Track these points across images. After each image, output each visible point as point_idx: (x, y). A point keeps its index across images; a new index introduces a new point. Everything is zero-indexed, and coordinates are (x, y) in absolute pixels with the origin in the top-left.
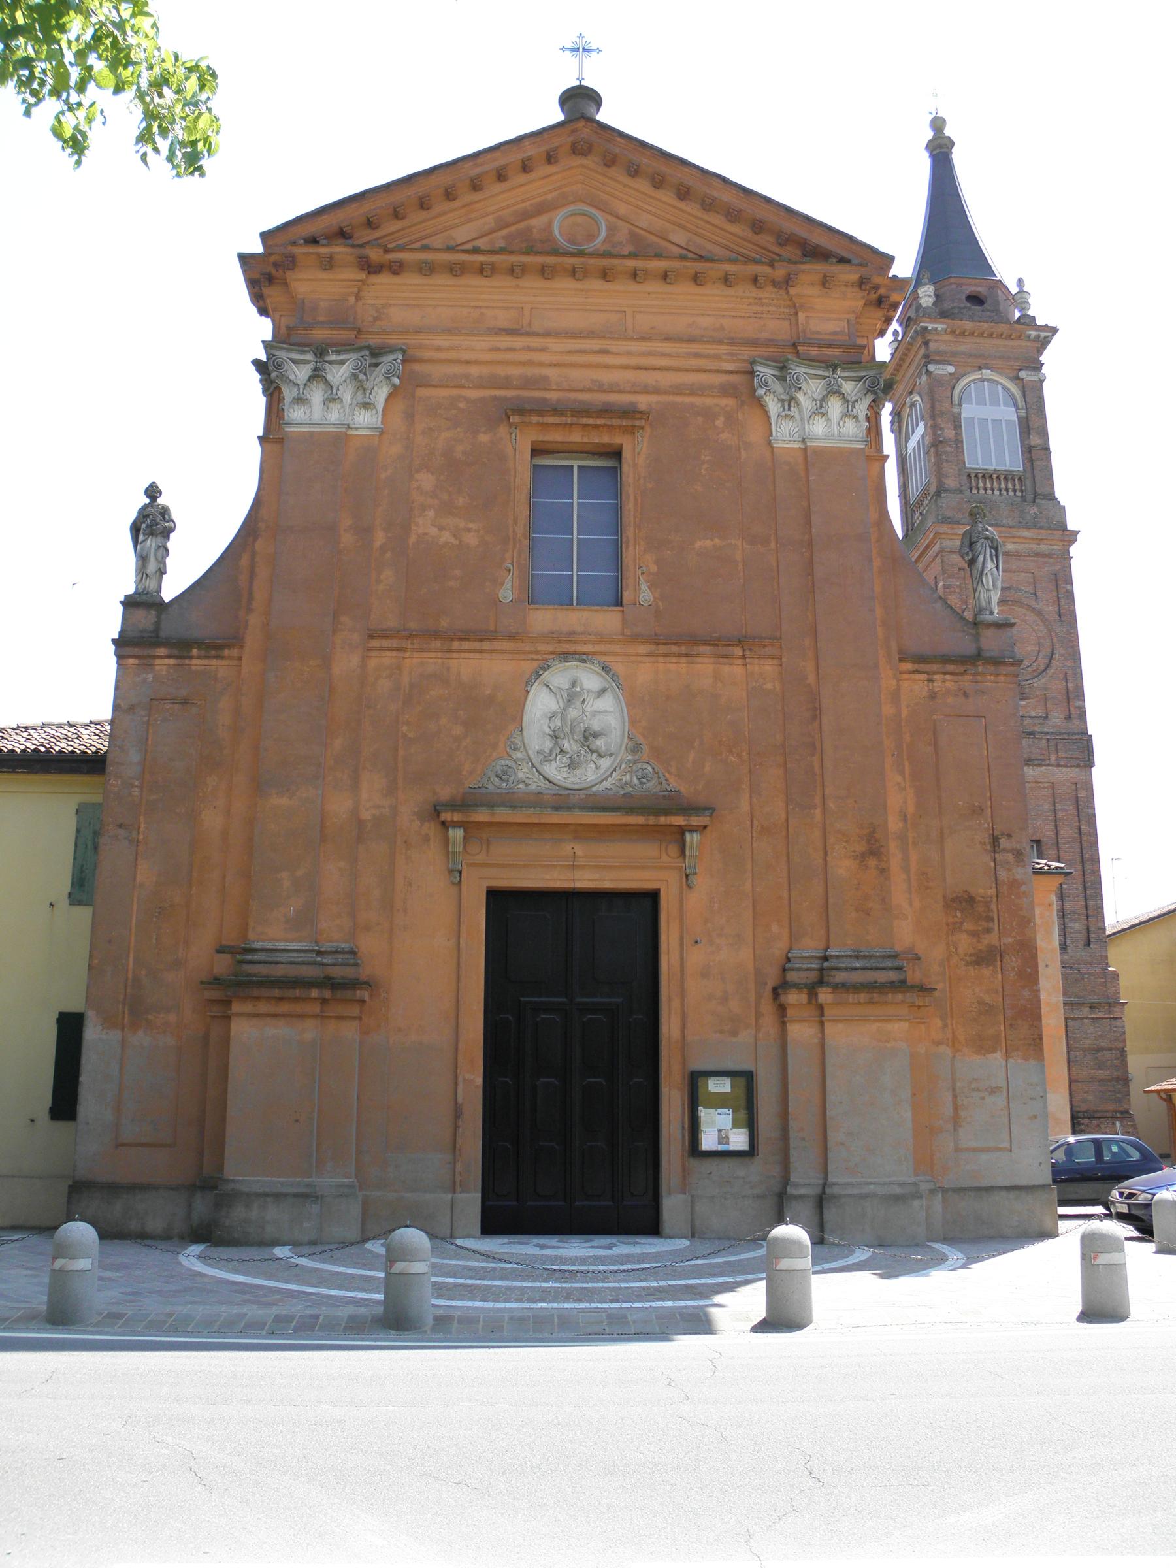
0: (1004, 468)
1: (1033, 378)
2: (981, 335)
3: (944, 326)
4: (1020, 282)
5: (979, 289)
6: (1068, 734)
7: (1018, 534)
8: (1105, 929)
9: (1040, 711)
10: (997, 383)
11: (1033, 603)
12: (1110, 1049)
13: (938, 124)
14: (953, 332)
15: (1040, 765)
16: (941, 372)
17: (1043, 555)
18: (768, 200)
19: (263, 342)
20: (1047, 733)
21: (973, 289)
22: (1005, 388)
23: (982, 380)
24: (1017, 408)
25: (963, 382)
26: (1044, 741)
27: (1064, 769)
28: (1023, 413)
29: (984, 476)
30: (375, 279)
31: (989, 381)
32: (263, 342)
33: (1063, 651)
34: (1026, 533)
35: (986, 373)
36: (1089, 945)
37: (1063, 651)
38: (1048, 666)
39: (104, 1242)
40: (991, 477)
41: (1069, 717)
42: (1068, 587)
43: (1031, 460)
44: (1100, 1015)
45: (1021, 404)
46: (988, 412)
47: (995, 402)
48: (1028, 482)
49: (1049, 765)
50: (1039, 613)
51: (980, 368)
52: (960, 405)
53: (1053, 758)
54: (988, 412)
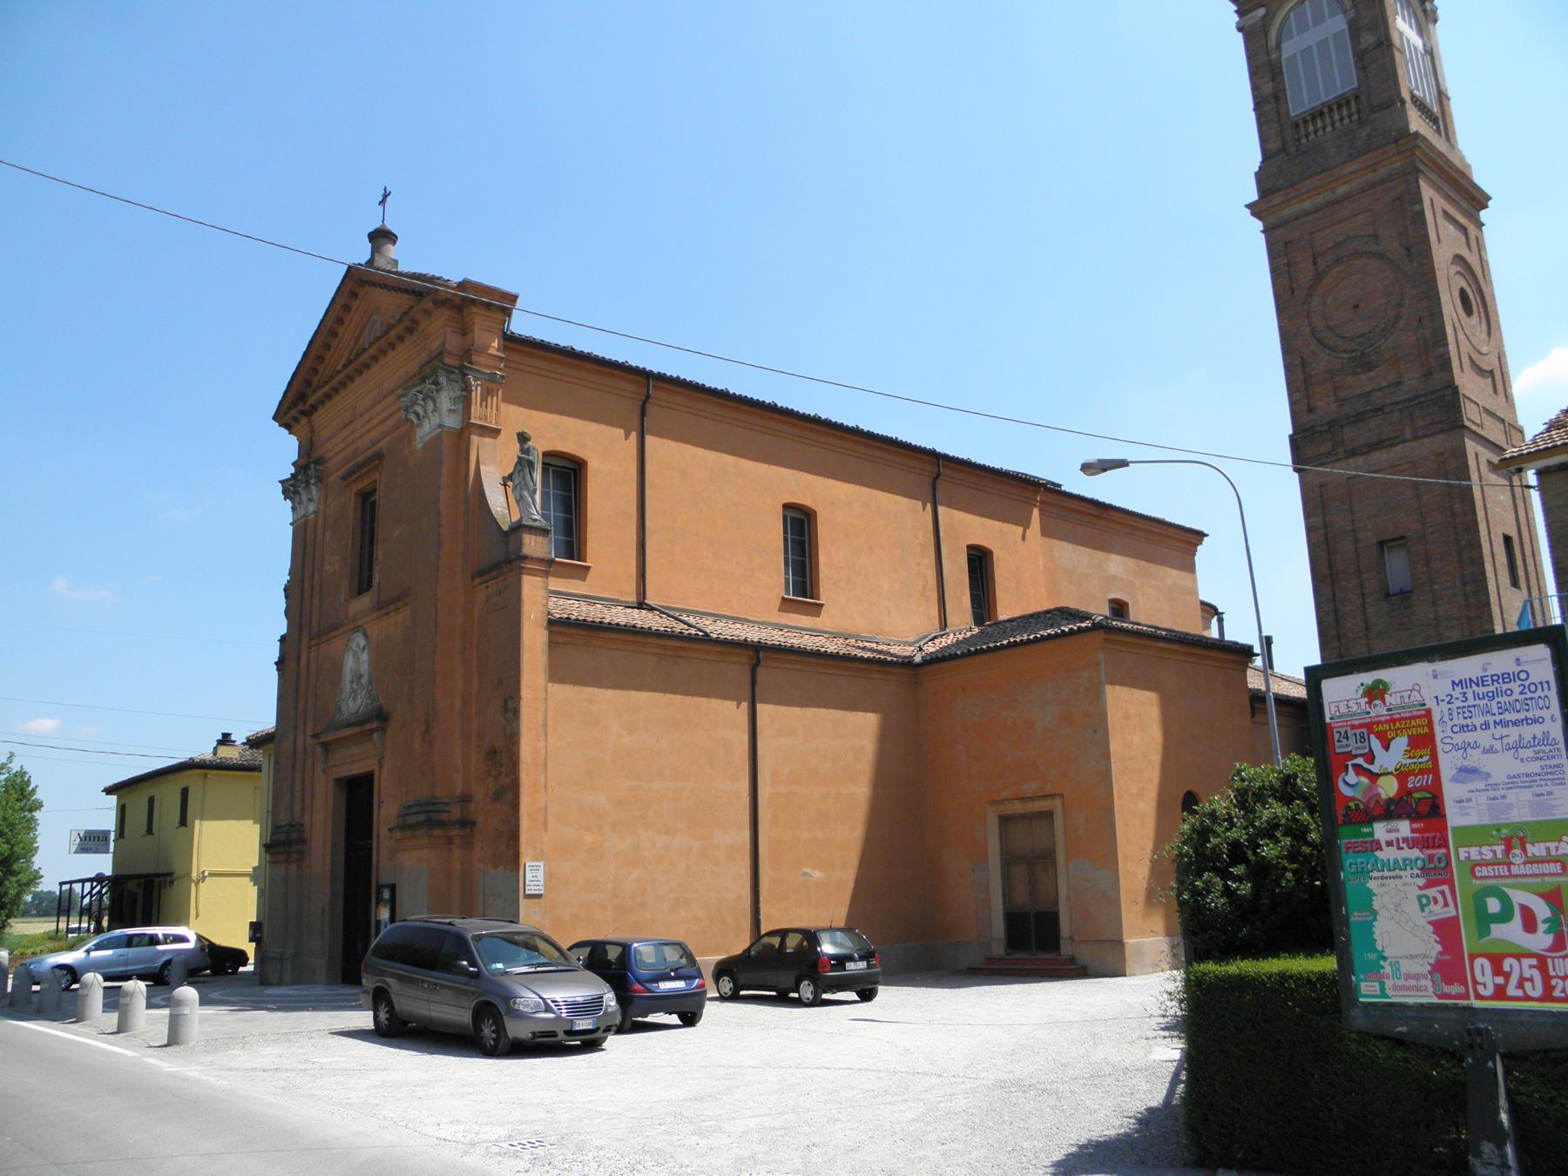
8: (1112, 683)
9: (1392, 378)
11: (1374, 248)
17: (1382, 182)
18: (311, 342)
24: (1345, 12)
25: (1279, 18)
27: (1425, 441)
28: (1352, 14)
29: (1314, 117)
30: (314, 417)
32: (1247, 206)
33: (1414, 292)
37: (1414, 292)
38: (1398, 317)
41: (1428, 375)
46: (1311, 37)
48: (1364, 98)
49: (1404, 441)
50: (1381, 256)
52: (1278, 47)
53: (1408, 431)
54: (1311, 37)
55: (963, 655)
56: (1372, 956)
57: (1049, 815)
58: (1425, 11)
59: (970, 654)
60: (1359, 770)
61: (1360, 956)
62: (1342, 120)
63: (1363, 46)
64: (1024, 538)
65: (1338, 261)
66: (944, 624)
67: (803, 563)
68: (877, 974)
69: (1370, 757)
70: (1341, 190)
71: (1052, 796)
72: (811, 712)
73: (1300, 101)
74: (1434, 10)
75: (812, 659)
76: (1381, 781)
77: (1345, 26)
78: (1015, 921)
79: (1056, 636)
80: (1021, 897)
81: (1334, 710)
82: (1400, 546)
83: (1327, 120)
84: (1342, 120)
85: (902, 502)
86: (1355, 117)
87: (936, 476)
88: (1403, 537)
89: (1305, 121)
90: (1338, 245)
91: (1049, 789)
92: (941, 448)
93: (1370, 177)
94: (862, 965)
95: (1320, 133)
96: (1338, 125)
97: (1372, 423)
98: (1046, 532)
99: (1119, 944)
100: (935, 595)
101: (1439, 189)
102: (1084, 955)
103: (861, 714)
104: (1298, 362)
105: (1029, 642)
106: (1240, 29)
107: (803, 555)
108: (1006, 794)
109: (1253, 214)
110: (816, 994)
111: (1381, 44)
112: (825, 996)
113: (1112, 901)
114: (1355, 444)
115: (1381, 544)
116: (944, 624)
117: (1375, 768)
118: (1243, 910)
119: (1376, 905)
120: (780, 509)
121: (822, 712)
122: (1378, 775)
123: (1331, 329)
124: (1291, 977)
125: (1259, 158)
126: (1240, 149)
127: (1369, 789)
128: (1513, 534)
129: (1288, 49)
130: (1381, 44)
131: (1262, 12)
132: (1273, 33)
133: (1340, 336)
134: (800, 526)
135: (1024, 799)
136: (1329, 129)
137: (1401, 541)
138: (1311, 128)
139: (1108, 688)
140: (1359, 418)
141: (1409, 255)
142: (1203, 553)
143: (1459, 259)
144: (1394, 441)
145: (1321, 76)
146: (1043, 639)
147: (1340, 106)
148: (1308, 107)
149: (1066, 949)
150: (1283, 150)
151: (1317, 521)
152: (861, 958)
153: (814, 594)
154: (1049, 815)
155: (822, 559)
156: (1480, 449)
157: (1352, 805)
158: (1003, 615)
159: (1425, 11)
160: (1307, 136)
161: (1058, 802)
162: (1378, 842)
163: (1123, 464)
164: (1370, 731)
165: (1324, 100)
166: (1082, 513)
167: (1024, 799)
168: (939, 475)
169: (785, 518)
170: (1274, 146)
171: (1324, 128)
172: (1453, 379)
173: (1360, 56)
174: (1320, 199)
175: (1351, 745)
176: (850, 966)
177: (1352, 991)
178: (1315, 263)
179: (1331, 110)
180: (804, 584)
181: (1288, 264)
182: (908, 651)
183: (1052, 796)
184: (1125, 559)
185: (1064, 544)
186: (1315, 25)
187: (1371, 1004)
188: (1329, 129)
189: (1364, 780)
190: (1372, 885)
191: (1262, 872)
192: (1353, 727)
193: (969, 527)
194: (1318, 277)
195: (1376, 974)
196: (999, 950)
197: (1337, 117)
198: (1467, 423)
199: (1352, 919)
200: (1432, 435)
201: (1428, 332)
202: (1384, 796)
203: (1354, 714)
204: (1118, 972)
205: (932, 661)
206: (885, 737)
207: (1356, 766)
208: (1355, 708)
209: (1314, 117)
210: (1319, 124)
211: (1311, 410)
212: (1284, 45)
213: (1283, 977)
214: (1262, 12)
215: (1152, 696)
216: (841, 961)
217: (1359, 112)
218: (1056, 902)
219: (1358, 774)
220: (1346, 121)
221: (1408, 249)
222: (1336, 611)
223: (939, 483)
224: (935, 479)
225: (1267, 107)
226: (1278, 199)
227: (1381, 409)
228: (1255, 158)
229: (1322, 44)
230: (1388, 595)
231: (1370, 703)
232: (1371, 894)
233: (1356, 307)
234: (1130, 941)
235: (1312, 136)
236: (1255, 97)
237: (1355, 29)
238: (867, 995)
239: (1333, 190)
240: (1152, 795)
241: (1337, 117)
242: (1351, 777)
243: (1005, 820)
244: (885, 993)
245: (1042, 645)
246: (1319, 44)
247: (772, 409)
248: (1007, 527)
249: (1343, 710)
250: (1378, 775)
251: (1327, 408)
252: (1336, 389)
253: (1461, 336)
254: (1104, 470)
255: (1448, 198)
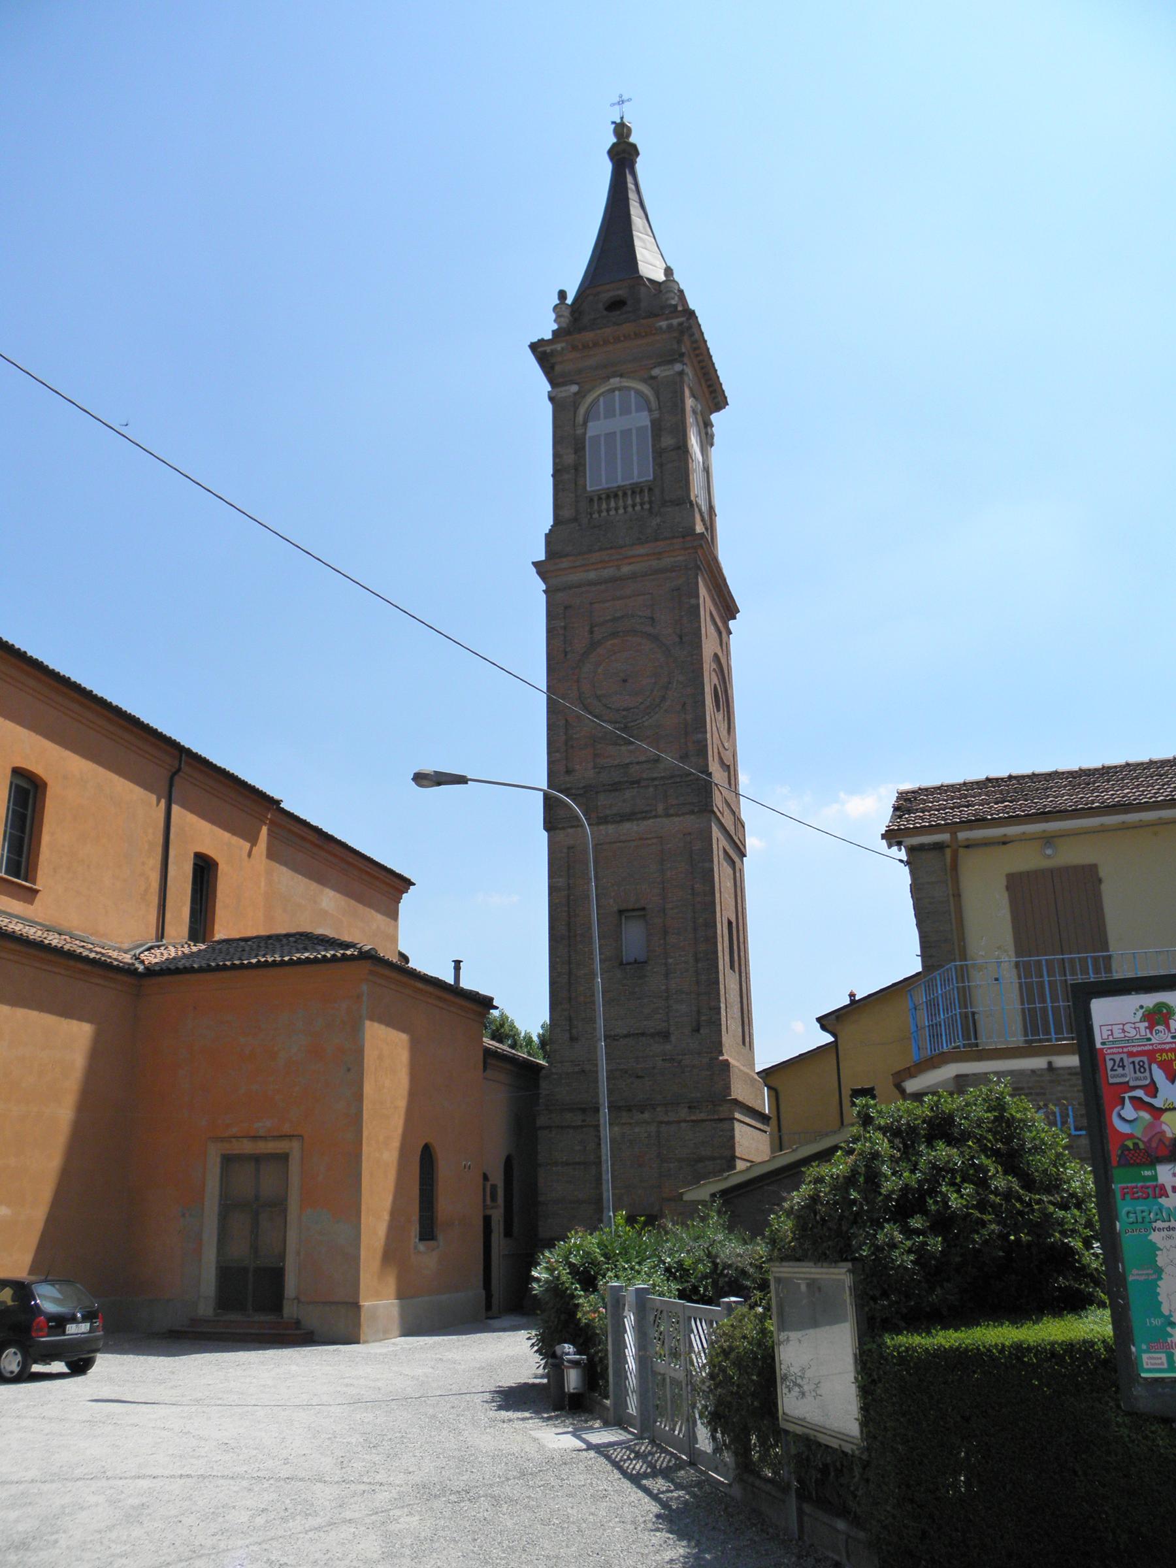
0: (615, 485)
1: (668, 373)
2: (606, 342)
3: (563, 345)
4: (668, 271)
5: (620, 292)
6: (681, 776)
7: (631, 553)
8: (372, 1019)
10: (629, 388)
11: (650, 630)
12: (713, 1159)
13: (622, 130)
14: (574, 348)
15: (644, 818)
16: (564, 395)
19: (535, 564)
20: (654, 779)
21: (611, 294)
22: (638, 392)
23: (613, 390)
24: (650, 410)
25: (589, 399)
26: (651, 789)
27: (676, 819)
28: (656, 415)
29: (608, 497)
31: (620, 389)
32: (535, 564)
34: (641, 550)
35: (615, 382)
36: (698, 1030)
38: (663, 699)
39: (362, 1337)
40: (616, 496)
42: (693, 601)
43: (661, 465)
44: (703, 1116)
45: (654, 405)
46: (618, 424)
47: (625, 411)
49: (656, 817)
50: (655, 638)
51: (608, 378)
52: (585, 423)
53: (660, 808)
54: (618, 424)
55: (201, 970)
56: (1156, 1322)
57: (284, 1158)
58: (707, 434)
59: (209, 969)
60: (1138, 1103)
61: (1139, 1320)
62: (634, 506)
63: (664, 445)
64: (249, 855)
65: (614, 635)
66: (161, 935)
67: (21, 840)
68: (97, 1339)
69: (1152, 1089)
70: (626, 569)
71: (290, 1137)
72: (21, 1013)
73: (597, 480)
74: (712, 436)
75: (33, 951)
76: (1166, 1117)
77: (647, 423)
78: (230, 1278)
79: (315, 961)
80: (239, 1250)
81: (1105, 1034)
82: (640, 916)
83: (621, 503)
84: (634, 506)
85: (138, 792)
86: (647, 506)
87: (179, 772)
88: (644, 909)
89: (600, 499)
90: (615, 620)
91: (287, 1128)
92: (185, 742)
93: (654, 563)
94: (85, 1327)
95: (612, 513)
96: (630, 509)
97: (628, 794)
98: (271, 855)
99: (356, 1306)
100: (155, 900)
101: (709, 591)
102: (312, 1319)
103: (75, 1022)
104: (562, 723)
105: (283, 963)
106: (551, 399)
107: (23, 831)
108: (234, 1130)
109: (539, 573)
110: (25, 1366)
111: (679, 448)
112: (36, 1368)
113: (353, 1260)
114: (608, 812)
115: (621, 912)
116: (161, 935)
117: (1158, 1102)
118: (932, 1269)
119: (1161, 1260)
120: (9, 772)
121: (34, 1015)
122: (1162, 1111)
123: (598, 698)
124: (1029, 1349)
125: (551, 522)
126: (538, 512)
127: (1151, 1126)
128: (733, 920)
129: (594, 429)
130: (679, 448)
131: (574, 388)
132: (582, 411)
133: (605, 705)
134: (28, 791)
135: (255, 1138)
136: (621, 511)
137: (640, 912)
138: (604, 506)
139: (368, 1023)
140: (615, 787)
141: (681, 642)
142: (407, 901)
143: (716, 655)
144: (644, 815)
145: (621, 464)
146: (300, 962)
147: (633, 492)
148: (604, 485)
149: (290, 1310)
150: (575, 520)
151: (561, 882)
152: (85, 1318)
153: (30, 875)
154: (284, 1158)
155: (46, 838)
156: (721, 838)
157: (1129, 1144)
158: (221, 933)
159: (707, 434)
160: (600, 512)
161: (295, 1144)
162: (1162, 1187)
163: (461, 780)
164: (1152, 1059)
165: (620, 483)
166: (304, 839)
167: (255, 1138)
168: (179, 770)
169: (11, 783)
170: (567, 513)
171: (616, 509)
172: (707, 765)
173: (659, 453)
174: (608, 573)
175: (1128, 1075)
176: (71, 1329)
177: (1131, 1364)
178: (591, 632)
179: (625, 494)
180: (19, 864)
181: (565, 628)
182: (127, 958)
183: (290, 1137)
184: (338, 895)
185: (284, 869)
186: (605, 418)
187: (1156, 1380)
188: (621, 511)
189: (1145, 1116)
190: (1155, 1237)
191: (943, 1223)
192: (1131, 1054)
193: (199, 833)
194: (593, 645)
195: (1160, 1342)
196: (206, 1309)
197: (630, 502)
198: (715, 809)
199: (1130, 1278)
200: (683, 814)
201: (689, 717)
202: (1169, 1135)
203: (1132, 1040)
204: (352, 1338)
205: (152, 972)
206: (96, 1053)
207: (1134, 1099)
208: (1133, 1032)
209: (608, 497)
210: (613, 504)
211: (568, 772)
212: (590, 424)
213: (1020, 1350)
214: (574, 388)
215: (404, 1037)
216: (60, 1322)
217: (650, 502)
218: (282, 1257)
219: (1136, 1108)
220: (638, 508)
221: (681, 637)
222: (570, 973)
223: (177, 779)
224: (175, 774)
225: (566, 477)
226: (565, 563)
227: (638, 782)
228: (546, 521)
229: (626, 433)
230: (621, 964)
231: (1151, 1028)
232: (1154, 1248)
233: (625, 681)
234: (366, 1303)
235: (604, 514)
236: (555, 464)
237: (657, 428)
238: (79, 1367)
239: (618, 567)
240: (396, 1144)
241: (630, 502)
242: (1129, 1111)
243: (228, 1160)
244: (105, 1364)
245: (299, 969)
246: (607, 435)
247: (21, 656)
248: (236, 841)
249: (1118, 1034)
250: (1162, 1111)
251: (585, 772)
252: (596, 756)
253: (714, 728)
254: (439, 784)
255: (715, 604)
